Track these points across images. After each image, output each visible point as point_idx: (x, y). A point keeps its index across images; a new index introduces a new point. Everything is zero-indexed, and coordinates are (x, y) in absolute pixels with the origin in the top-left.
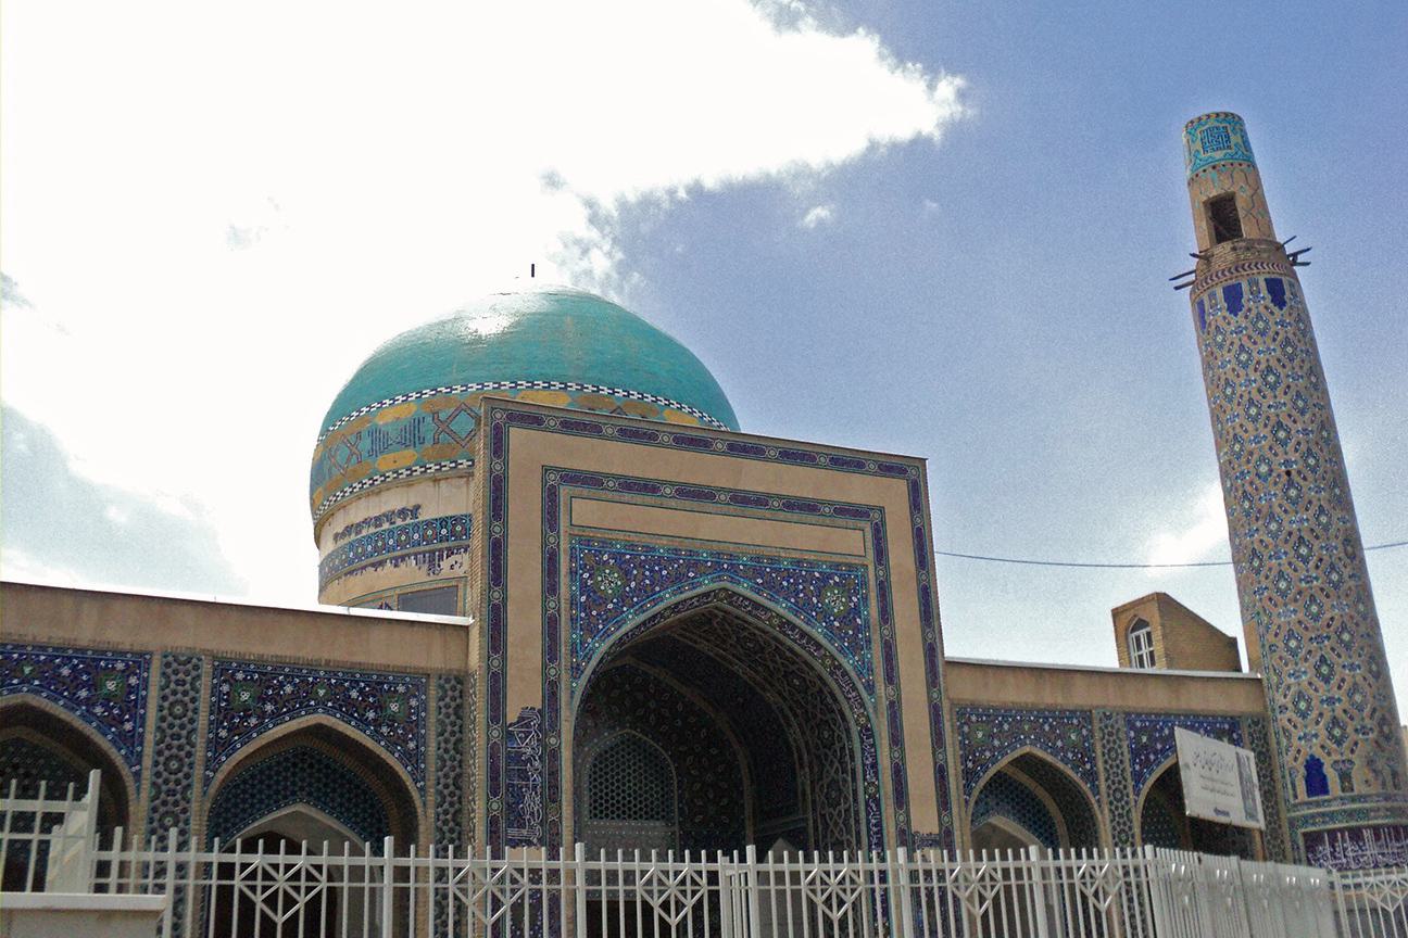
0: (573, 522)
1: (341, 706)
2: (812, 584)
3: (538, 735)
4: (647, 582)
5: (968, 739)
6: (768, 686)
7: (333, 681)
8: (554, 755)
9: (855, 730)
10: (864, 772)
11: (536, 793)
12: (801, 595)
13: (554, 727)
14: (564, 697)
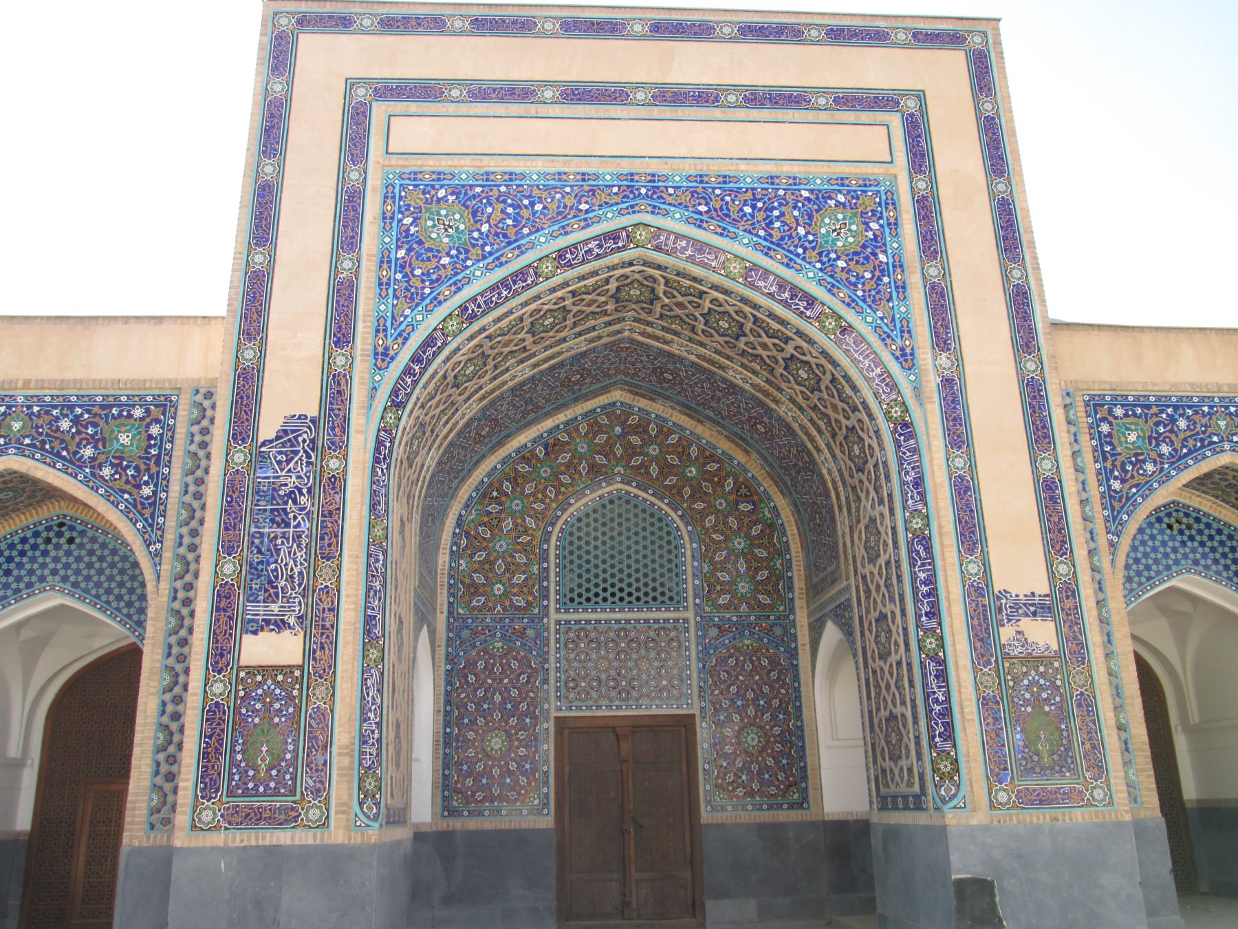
0: (390, 150)
1: (43, 442)
2: (795, 207)
3: (309, 457)
4: (510, 222)
5: (1110, 443)
6: (669, 336)
7: (36, 409)
8: (336, 483)
9: (885, 428)
10: (904, 494)
11: (299, 546)
12: (777, 224)
13: (340, 445)
14: (358, 394)
